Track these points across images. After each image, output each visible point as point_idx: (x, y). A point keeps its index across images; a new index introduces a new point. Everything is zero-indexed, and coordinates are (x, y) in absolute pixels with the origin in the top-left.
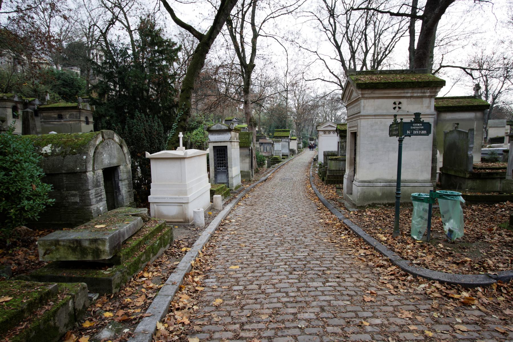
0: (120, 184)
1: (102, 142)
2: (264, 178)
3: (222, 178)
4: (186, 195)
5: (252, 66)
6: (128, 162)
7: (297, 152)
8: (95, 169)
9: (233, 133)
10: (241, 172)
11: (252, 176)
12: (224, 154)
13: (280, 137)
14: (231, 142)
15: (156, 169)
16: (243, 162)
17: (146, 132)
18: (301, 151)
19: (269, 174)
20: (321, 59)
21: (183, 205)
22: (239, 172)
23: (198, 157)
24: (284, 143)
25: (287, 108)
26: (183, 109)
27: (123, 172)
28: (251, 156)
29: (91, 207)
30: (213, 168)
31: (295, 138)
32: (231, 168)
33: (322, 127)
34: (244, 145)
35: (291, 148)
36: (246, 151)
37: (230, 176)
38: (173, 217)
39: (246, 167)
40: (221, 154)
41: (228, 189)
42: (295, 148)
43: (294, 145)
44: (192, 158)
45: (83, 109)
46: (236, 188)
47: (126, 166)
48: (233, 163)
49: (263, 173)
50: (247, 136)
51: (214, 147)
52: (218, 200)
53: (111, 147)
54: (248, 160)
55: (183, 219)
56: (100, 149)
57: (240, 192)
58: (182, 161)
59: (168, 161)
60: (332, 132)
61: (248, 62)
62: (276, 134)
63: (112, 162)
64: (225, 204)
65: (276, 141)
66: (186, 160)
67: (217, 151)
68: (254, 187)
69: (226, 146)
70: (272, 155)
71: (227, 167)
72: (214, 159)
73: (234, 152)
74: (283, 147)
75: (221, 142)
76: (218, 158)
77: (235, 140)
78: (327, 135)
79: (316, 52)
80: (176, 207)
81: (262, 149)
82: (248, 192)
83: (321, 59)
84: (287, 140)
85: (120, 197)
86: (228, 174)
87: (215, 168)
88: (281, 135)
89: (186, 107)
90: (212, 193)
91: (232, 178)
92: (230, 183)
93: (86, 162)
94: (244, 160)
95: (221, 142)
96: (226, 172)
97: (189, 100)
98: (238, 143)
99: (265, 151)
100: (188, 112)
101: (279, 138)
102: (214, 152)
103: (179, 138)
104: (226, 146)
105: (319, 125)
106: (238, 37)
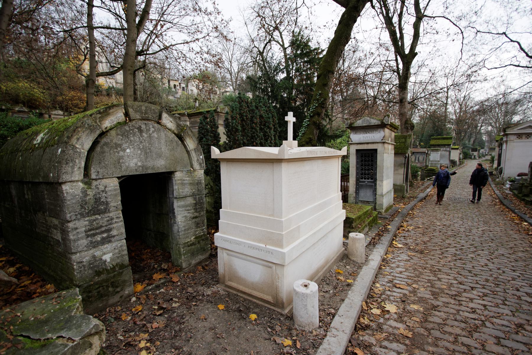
0: (176, 204)
1: (119, 124)
2: (422, 195)
3: (366, 195)
4: (280, 245)
5: (413, 54)
6: (196, 166)
7: (458, 163)
8: (93, 176)
9: (387, 130)
10: (394, 185)
11: (407, 191)
12: (372, 161)
13: (439, 146)
14: (384, 143)
15: (231, 180)
16: (396, 172)
17: (243, 120)
18: (463, 163)
19: (429, 190)
20: (512, 41)
21: (274, 267)
22: (392, 186)
23: (320, 162)
24: (444, 153)
25: (445, 116)
26: (318, 100)
27: (183, 184)
28: (407, 165)
29: (74, 257)
30: (354, 179)
31: (457, 147)
32: (382, 181)
33: (515, 129)
34: (399, 152)
35: (451, 159)
36: (401, 159)
37: (379, 192)
38: (253, 286)
39: (400, 179)
40: (368, 159)
41: (375, 213)
42: (457, 159)
43: (455, 155)
44: (306, 163)
45: (221, 113)
46: (387, 210)
47: (191, 172)
48: (384, 175)
49: (419, 187)
50: (403, 140)
51: (357, 151)
52: (357, 245)
53: (150, 136)
54: (402, 171)
55: (273, 298)
56: (114, 137)
57: (393, 216)
58: (276, 165)
59: (249, 166)
60: (524, 137)
61: (407, 51)
62: (432, 142)
63: (150, 164)
64: (370, 244)
65: (433, 150)
66: (284, 165)
67: (362, 156)
68: (412, 209)
69: (376, 150)
70: (427, 166)
71: (376, 180)
72: (357, 168)
73: (387, 159)
74: (442, 157)
75: (368, 143)
76: (362, 165)
77: (390, 142)
78: (524, 140)
79: (504, 33)
80: (261, 267)
81: (413, 159)
82: (407, 216)
83: (512, 41)
84: (448, 149)
85: (175, 228)
86: (375, 190)
87: (357, 180)
88: (439, 143)
89: (321, 98)
90: (349, 225)
91: (382, 196)
92: (378, 202)
93: (59, 162)
94: (397, 170)
95: (368, 143)
96: (374, 187)
97: (326, 88)
98: (393, 147)
99: (417, 161)
100: (324, 104)
101: (436, 147)
102: (357, 158)
103: (286, 123)
104: (376, 150)
105: (509, 127)
106: (395, 19)
